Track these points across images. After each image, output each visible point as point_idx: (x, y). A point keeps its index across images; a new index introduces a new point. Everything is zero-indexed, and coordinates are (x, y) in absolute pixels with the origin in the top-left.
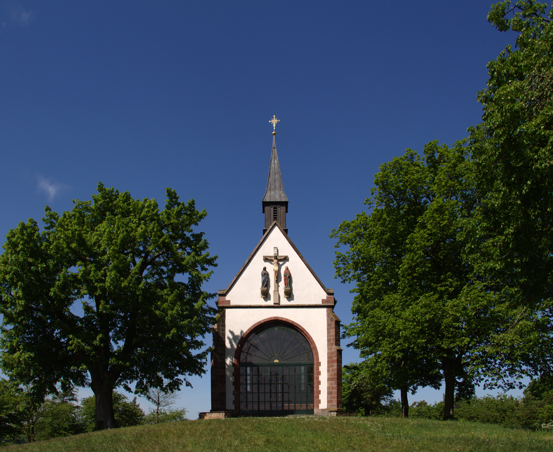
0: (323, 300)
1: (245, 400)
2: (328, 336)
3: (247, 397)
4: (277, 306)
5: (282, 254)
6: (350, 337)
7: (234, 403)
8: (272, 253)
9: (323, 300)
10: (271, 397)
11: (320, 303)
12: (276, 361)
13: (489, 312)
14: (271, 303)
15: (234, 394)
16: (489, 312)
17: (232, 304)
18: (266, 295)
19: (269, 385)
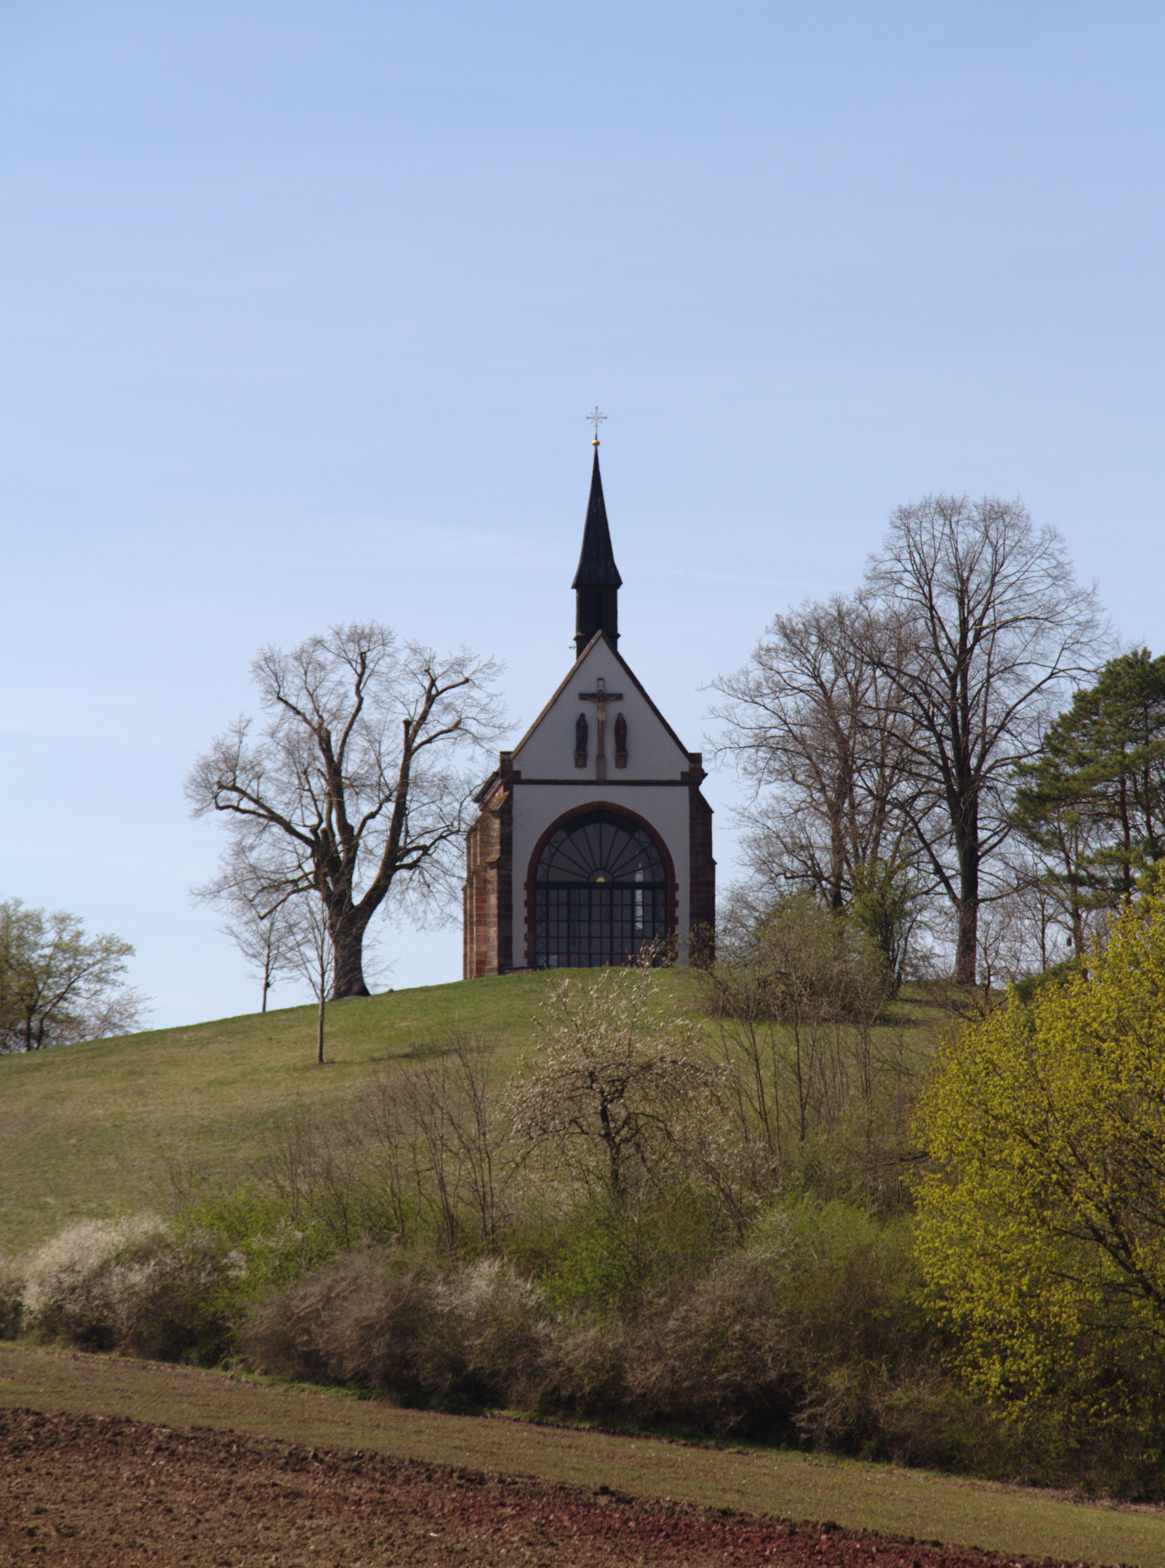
0: (683, 774)
1: (544, 934)
2: (691, 838)
3: (547, 929)
4: (601, 782)
5: (611, 689)
6: (866, 568)
7: (527, 954)
8: (592, 689)
9: (683, 774)
10: (590, 946)
11: (678, 778)
12: (601, 880)
13: (1057, 760)
14: (589, 773)
15: (526, 939)
16: (1057, 760)
17: (524, 776)
18: (581, 758)
19: (587, 924)
